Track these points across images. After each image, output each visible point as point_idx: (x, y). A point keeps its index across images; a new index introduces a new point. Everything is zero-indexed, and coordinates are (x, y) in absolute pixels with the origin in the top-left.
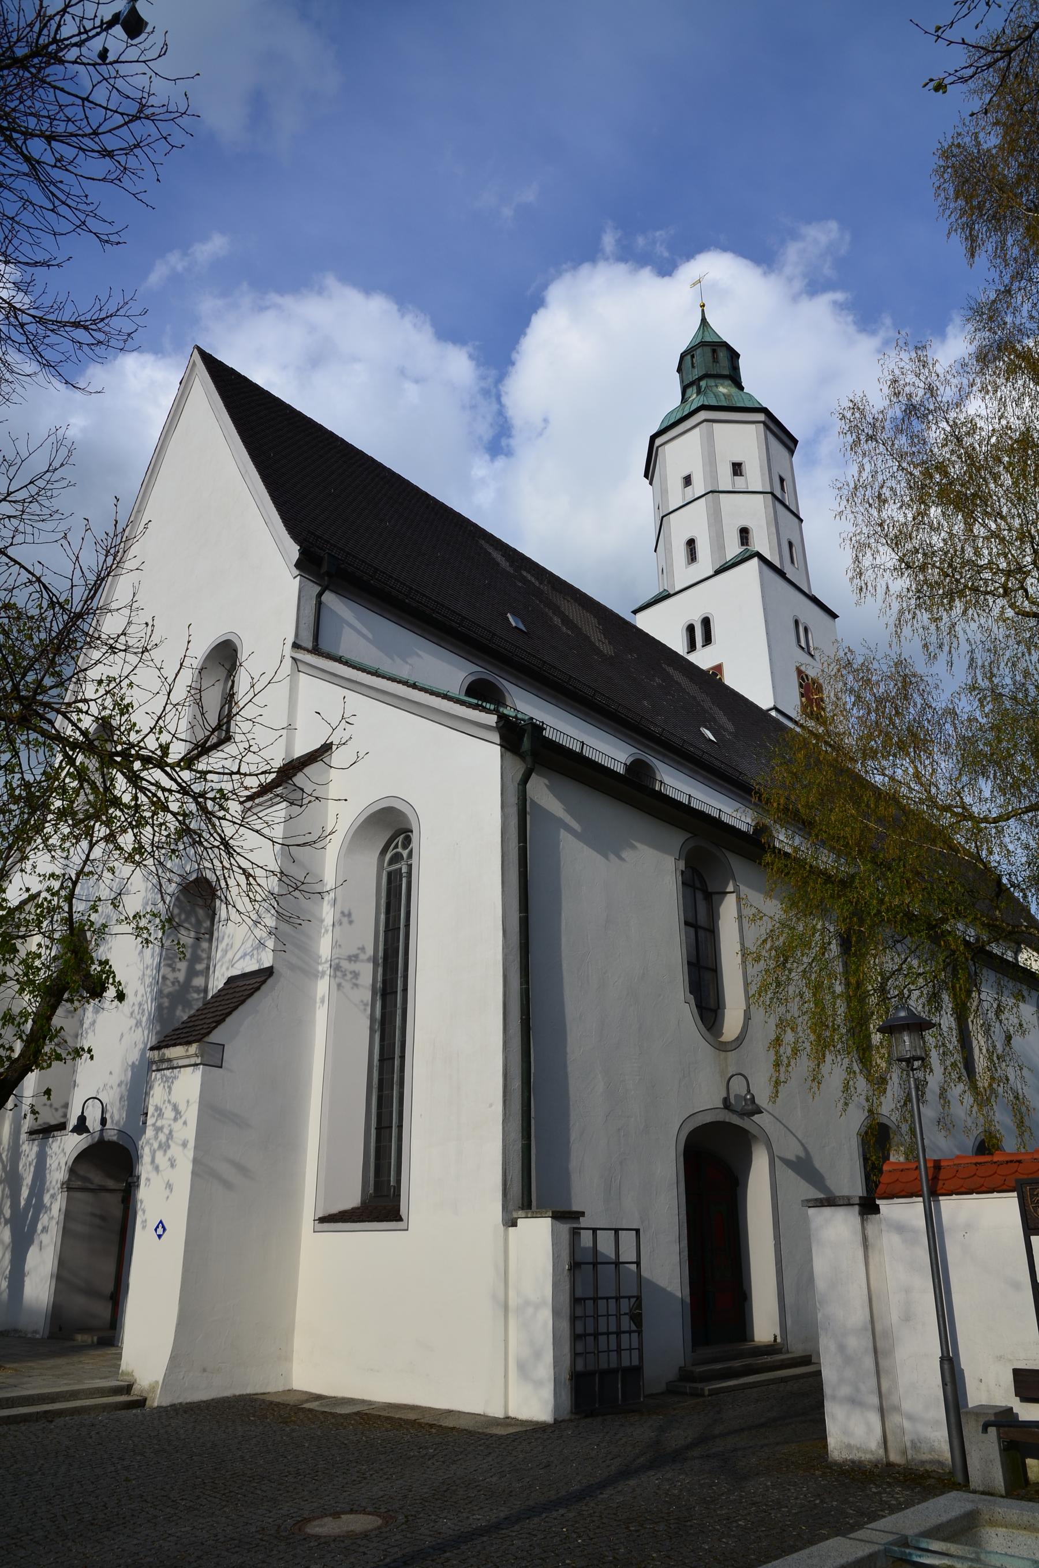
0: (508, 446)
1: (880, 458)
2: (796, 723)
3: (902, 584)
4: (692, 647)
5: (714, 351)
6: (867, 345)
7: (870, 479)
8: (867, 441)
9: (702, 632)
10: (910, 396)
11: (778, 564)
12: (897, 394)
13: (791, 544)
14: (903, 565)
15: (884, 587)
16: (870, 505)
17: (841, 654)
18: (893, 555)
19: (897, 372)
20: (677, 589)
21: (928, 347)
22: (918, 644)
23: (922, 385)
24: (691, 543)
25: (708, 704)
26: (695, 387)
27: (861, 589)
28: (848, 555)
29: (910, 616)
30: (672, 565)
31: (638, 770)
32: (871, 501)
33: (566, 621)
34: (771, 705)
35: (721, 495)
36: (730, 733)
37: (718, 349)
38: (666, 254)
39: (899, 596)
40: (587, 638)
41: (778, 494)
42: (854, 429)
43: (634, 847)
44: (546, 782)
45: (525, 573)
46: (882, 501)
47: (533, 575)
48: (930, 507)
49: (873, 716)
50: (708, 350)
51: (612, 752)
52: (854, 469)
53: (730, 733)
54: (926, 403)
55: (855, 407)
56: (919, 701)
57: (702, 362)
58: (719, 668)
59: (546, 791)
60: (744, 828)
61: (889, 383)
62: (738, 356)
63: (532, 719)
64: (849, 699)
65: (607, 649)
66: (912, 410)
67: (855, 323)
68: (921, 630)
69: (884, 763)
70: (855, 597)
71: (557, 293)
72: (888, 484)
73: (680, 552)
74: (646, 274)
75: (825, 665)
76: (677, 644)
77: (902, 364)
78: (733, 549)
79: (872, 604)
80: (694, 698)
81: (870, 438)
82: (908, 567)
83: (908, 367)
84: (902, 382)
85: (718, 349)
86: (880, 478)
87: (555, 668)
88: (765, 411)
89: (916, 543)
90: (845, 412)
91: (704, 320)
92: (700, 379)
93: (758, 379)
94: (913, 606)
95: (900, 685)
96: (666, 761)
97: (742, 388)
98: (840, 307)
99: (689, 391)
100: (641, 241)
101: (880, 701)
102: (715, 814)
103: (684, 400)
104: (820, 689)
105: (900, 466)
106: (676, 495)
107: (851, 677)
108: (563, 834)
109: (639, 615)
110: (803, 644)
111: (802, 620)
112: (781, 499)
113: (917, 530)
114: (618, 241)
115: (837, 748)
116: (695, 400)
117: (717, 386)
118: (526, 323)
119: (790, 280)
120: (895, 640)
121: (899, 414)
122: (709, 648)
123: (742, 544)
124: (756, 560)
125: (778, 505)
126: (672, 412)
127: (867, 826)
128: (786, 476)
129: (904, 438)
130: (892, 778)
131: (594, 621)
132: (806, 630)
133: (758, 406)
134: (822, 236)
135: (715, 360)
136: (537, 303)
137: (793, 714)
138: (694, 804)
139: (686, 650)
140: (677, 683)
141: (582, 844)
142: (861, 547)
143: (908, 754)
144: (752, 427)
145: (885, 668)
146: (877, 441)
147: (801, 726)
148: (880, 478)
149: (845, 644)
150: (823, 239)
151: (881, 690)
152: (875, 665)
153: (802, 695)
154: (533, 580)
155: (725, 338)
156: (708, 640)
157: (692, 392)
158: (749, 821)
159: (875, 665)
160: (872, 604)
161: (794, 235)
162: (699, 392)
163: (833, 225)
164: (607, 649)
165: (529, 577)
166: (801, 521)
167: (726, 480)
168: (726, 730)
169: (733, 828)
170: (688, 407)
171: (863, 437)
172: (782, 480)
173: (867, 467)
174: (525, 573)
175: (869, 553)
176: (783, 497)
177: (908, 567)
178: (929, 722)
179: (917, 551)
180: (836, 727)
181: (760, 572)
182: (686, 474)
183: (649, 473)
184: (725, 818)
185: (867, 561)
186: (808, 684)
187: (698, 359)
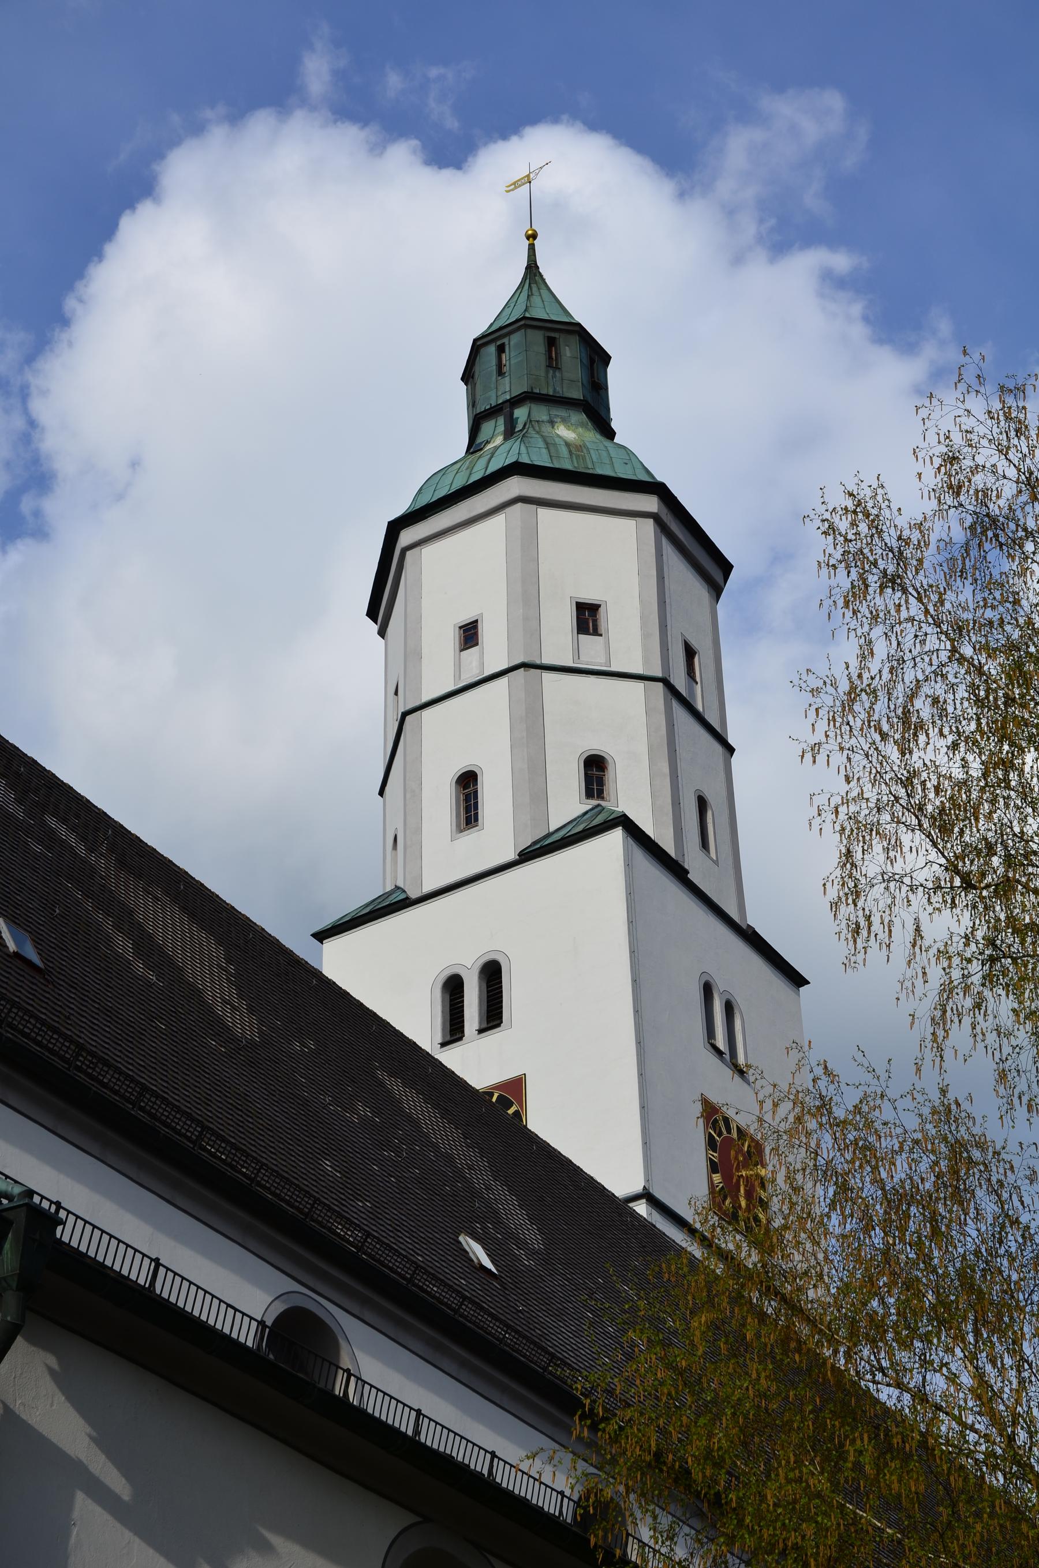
0: (37, 513)
1: (910, 630)
2: (692, 1231)
3: (951, 924)
4: (454, 1030)
5: (551, 343)
6: (894, 373)
7: (886, 676)
8: (882, 588)
9: (479, 996)
10: (984, 496)
11: (668, 845)
12: (956, 490)
13: (702, 804)
14: (957, 882)
15: (911, 928)
16: (884, 736)
17: (805, 1080)
18: (933, 855)
19: (957, 439)
20: (428, 888)
21: (1029, 389)
22: (985, 1067)
23: (1012, 473)
24: (468, 781)
25: (481, 1177)
26: (501, 420)
27: (857, 930)
28: (832, 846)
29: (968, 1003)
30: (419, 830)
31: (298, 1338)
32: (885, 727)
33: (146, 946)
34: (637, 1187)
35: (547, 676)
36: (533, 1253)
37: (561, 339)
38: (452, 123)
39: (943, 953)
40: (195, 994)
41: (680, 682)
42: (854, 559)
43: (265, 1548)
44: (52, 1361)
45: (52, 822)
46: (910, 726)
47: (73, 829)
48: (1022, 750)
49: (877, 1237)
50: (538, 338)
51: (231, 1289)
52: (848, 650)
53: (533, 1253)
54: (1019, 513)
55: (858, 509)
56: (990, 1207)
57: (523, 362)
58: (515, 1087)
59: (48, 1385)
60: (550, 1505)
61: (937, 462)
62: (605, 358)
63: (30, 1193)
64: (822, 1194)
65: (243, 1024)
66: (986, 526)
67: (866, 319)
68: (992, 1038)
69: (903, 1356)
70: (843, 948)
71: (185, 169)
72: (926, 689)
73: (439, 801)
74: (402, 155)
75: (768, 1105)
76: (418, 1022)
77: (968, 423)
78: (567, 804)
79: (884, 968)
80: (449, 1159)
81: (892, 581)
82: (968, 885)
83: (982, 430)
84: (967, 463)
85: (561, 339)
86: (909, 676)
87: (106, 1063)
88: (660, 490)
89: (984, 828)
90: (836, 519)
91: (532, 270)
92: (516, 402)
93: (648, 416)
94: (976, 979)
95: (943, 1164)
96: (368, 1316)
97: (609, 434)
98: (833, 283)
99: (487, 428)
100: (394, 81)
101: (899, 1201)
102: (480, 1464)
103: (474, 446)
104: (755, 1154)
105: (954, 650)
106: (440, 667)
107: (827, 1139)
108: (83, 1505)
109: (332, 946)
110: (721, 1042)
111: (720, 985)
112: (686, 694)
113: (993, 801)
114: (339, 76)
115: (792, 1306)
116: (501, 449)
117: (552, 423)
118: (108, 230)
119: (730, 212)
120: (929, 1055)
121: (959, 535)
122: (494, 1037)
123: (589, 794)
124: (617, 835)
125: (680, 714)
126: (443, 471)
127: (856, 1520)
128: (702, 645)
129: (969, 589)
130: (921, 1396)
131: (217, 952)
132: (729, 1008)
133: (643, 477)
134: (807, 121)
135: (553, 363)
136: (138, 187)
137: (688, 1215)
138: (430, 1437)
139: (439, 1039)
140: (410, 1119)
141: (128, 1535)
142: (858, 832)
143: (960, 1337)
144: (629, 524)
145: (911, 1122)
146: (905, 591)
147: (706, 1242)
148: (909, 676)
149: (814, 1057)
150: (811, 131)
151: (900, 1175)
152: (887, 1113)
153: (713, 1167)
154: (72, 840)
155: (580, 316)
156: (493, 1016)
157: (494, 431)
158: (562, 1483)
159: (887, 1113)
160: (884, 968)
161: (747, 114)
162: (510, 432)
163: (834, 101)
164: (243, 1024)
165: (63, 831)
166: (731, 750)
167: (559, 641)
168: (521, 1244)
169: (522, 1503)
170: (482, 463)
171: (873, 579)
172: (690, 653)
173: (881, 649)
174: (52, 822)
175: (878, 847)
176: (692, 692)
177: (968, 885)
178: (1012, 1259)
179: (991, 850)
180: (786, 1257)
181: (628, 865)
182: (466, 618)
183: (379, 608)
184: (504, 1478)
185: (873, 863)
186: (728, 1141)
187: (512, 358)
